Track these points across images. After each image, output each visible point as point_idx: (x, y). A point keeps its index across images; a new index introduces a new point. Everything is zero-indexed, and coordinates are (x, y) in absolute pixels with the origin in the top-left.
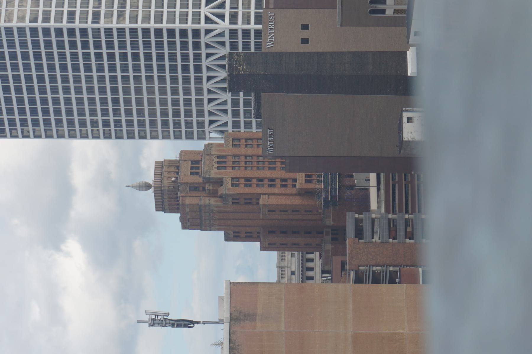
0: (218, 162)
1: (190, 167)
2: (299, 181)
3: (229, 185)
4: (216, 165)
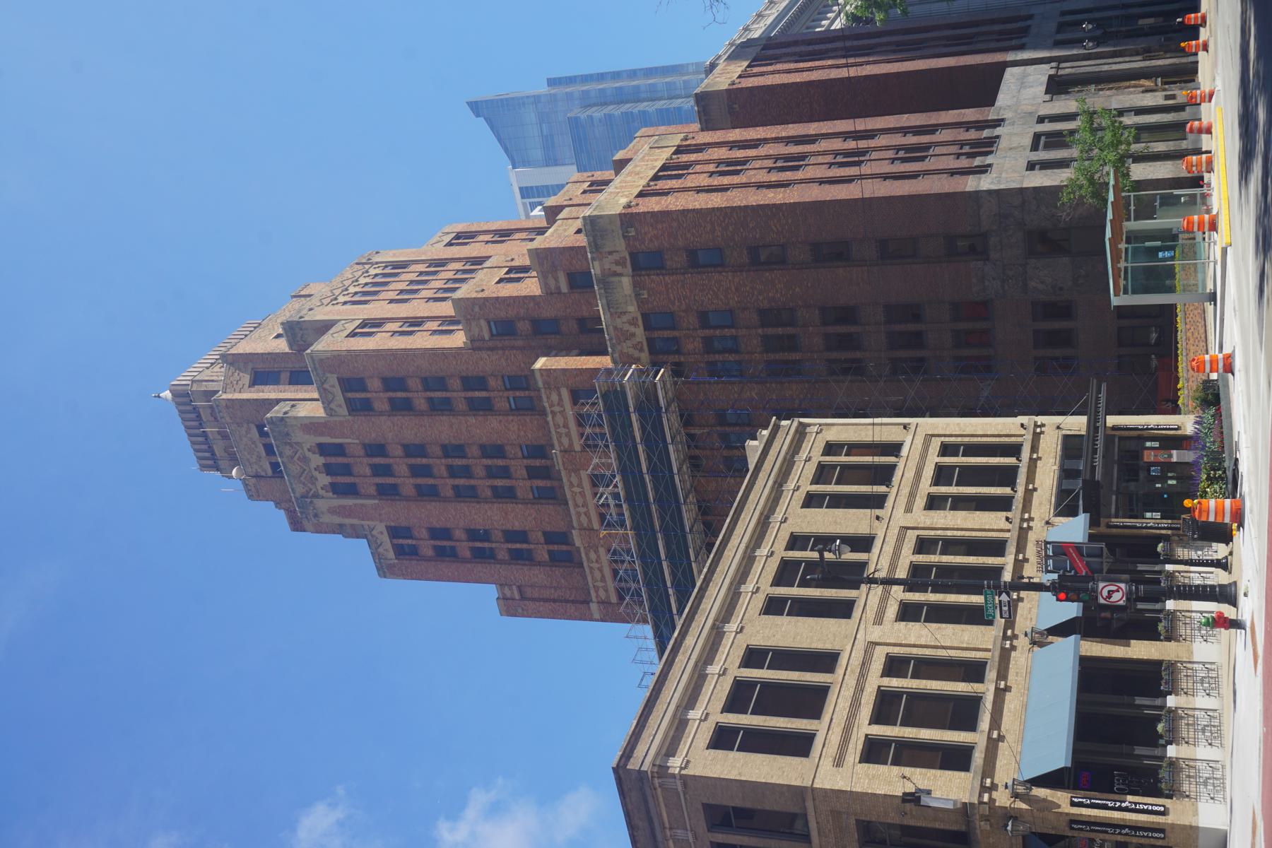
0: (329, 469)
1: (261, 445)
2: (597, 592)
3: (386, 550)
4: (324, 480)
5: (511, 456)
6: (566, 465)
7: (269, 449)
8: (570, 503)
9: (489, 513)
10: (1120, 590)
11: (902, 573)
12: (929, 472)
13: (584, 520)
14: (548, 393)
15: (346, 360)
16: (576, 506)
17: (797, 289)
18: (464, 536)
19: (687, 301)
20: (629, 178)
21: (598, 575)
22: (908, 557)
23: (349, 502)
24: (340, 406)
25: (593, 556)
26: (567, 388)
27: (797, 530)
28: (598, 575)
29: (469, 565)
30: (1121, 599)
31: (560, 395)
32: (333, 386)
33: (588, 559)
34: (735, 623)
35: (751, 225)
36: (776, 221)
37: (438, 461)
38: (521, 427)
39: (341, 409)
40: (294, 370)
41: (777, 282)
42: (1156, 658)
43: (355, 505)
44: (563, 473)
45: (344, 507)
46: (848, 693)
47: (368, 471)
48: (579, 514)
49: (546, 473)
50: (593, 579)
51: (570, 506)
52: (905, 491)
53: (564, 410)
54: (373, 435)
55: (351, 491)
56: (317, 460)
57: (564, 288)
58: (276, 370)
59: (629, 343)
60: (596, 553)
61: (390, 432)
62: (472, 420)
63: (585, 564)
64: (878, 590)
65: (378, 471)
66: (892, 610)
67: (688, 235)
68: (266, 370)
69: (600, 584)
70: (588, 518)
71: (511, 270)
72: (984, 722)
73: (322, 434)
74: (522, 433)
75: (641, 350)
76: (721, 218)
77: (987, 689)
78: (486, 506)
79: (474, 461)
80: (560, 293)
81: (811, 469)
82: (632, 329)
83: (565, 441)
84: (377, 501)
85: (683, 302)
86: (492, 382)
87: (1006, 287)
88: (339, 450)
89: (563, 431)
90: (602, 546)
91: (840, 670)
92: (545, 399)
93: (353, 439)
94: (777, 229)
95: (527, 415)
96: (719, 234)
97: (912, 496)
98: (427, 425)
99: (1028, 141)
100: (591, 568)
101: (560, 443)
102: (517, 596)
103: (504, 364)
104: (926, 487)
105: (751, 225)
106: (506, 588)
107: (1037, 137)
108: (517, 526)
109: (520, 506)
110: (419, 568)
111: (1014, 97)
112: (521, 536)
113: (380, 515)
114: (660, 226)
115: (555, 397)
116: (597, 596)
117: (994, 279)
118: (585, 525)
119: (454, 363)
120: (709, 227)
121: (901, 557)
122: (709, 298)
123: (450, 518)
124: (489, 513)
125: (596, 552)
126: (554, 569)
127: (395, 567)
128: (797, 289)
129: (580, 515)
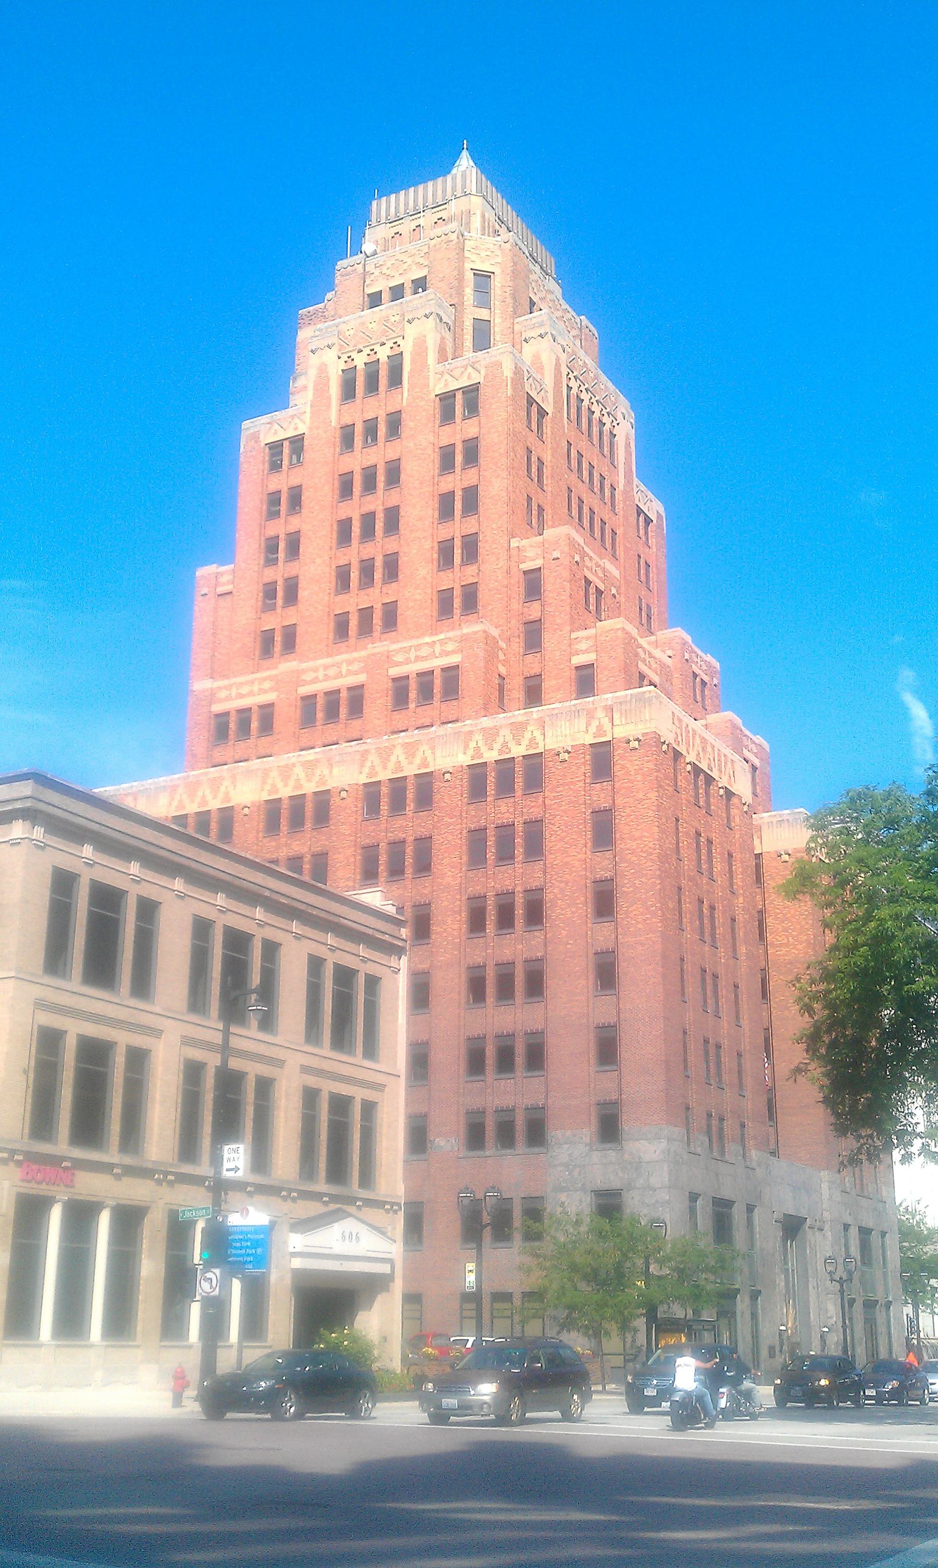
4: (360, 361)
5: (384, 590)
6: (373, 657)
7: (397, 292)
8: (329, 661)
9: (318, 561)
10: (212, 1290)
11: (234, 1064)
12: (344, 1089)
13: (308, 677)
14: (456, 639)
15: (500, 394)
16: (326, 667)
17: (564, 933)
18: (292, 529)
19: (555, 806)
20: (698, 740)
21: (245, 690)
22: (253, 1070)
23: (335, 390)
24: (446, 385)
25: (267, 685)
26: (462, 662)
27: (283, 951)
28: (245, 690)
29: (257, 533)
30: (206, 1292)
31: (454, 652)
32: (469, 377)
33: (265, 679)
34: (184, 888)
35: (637, 882)
36: (641, 910)
37: (380, 502)
38: (418, 603)
39: (443, 385)
40: (492, 325)
41: (574, 909)
42: (188, 970)
43: (329, 398)
44: (363, 653)
45: (327, 385)
46: (111, 1011)
47: (370, 415)
48: (315, 670)
49: (366, 628)
50: (239, 683)
51: (326, 659)
52: (326, 1066)
53: (437, 657)
54: (411, 424)
55: (348, 391)
56: (383, 354)
57: (577, 660)
58: (492, 302)
59: (509, 737)
60: (270, 688)
61: (415, 445)
62: (427, 544)
63: (258, 675)
64: (218, 1038)
65: (371, 429)
66: (197, 1054)
67: (628, 810)
68: (492, 291)
69: (234, 692)
70: (311, 681)
71: (599, 592)
72: (78, 1153)
73: (413, 361)
74: (411, 604)
75: (501, 752)
76: (646, 849)
77: (112, 1155)
78: (327, 558)
79: (379, 545)
80: (572, 654)
81: (349, 961)
82: (525, 742)
83: (399, 658)
84: (333, 424)
85: (554, 802)
86: (471, 570)
87: (559, 1169)
88: (396, 379)
89: (412, 655)
90: (278, 696)
91: (133, 1002)
92: (451, 634)
93: (407, 399)
94: (632, 911)
95: (432, 611)
96: (628, 846)
97: (320, 1073)
98: (421, 491)
99: (726, 1193)
100: (252, 682)
101: (398, 651)
102: (220, 590)
103: (491, 586)
104: (329, 1087)
105: (637, 882)
106: (230, 577)
107: (729, 1204)
108: (303, 594)
109: (327, 598)
110: (255, 472)
111: (783, 1179)
112: (292, 595)
113: (318, 428)
114: (639, 778)
115: (450, 647)
116: (220, 688)
117: (570, 1155)
118: (303, 677)
119: (494, 526)
120: (637, 834)
121: (252, 1063)
122: (557, 831)
123: (313, 513)
124: (318, 561)
125: (272, 689)
126: (252, 635)
127: (256, 442)
128: (564, 933)
129: (314, 671)
